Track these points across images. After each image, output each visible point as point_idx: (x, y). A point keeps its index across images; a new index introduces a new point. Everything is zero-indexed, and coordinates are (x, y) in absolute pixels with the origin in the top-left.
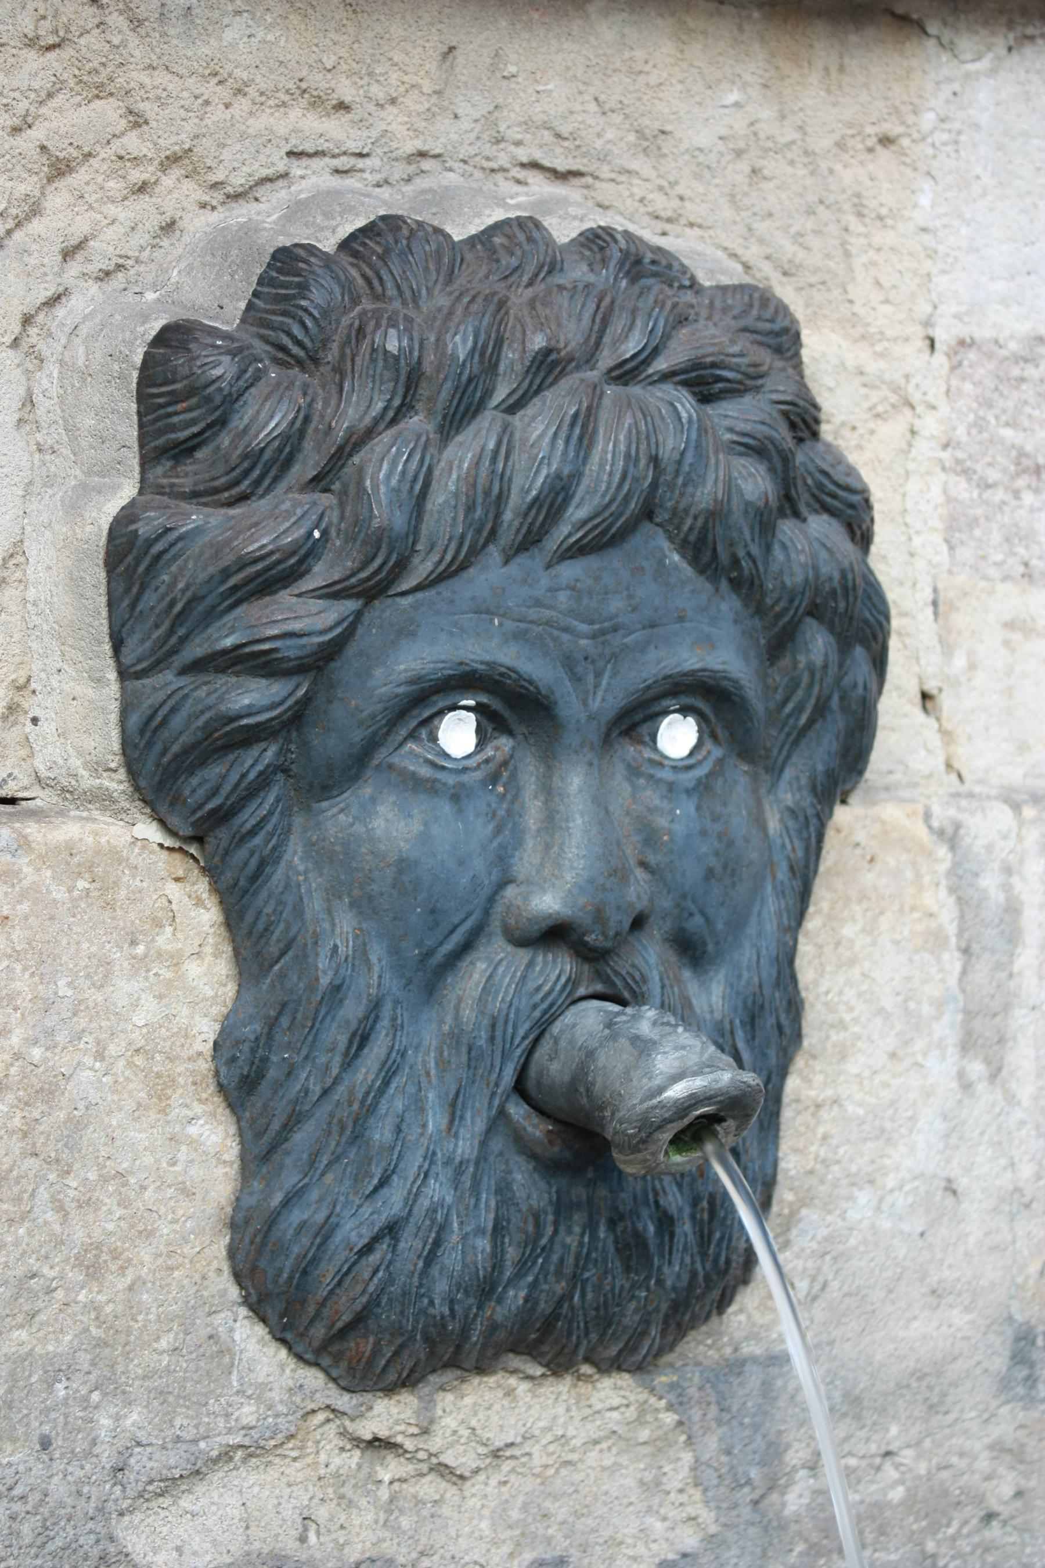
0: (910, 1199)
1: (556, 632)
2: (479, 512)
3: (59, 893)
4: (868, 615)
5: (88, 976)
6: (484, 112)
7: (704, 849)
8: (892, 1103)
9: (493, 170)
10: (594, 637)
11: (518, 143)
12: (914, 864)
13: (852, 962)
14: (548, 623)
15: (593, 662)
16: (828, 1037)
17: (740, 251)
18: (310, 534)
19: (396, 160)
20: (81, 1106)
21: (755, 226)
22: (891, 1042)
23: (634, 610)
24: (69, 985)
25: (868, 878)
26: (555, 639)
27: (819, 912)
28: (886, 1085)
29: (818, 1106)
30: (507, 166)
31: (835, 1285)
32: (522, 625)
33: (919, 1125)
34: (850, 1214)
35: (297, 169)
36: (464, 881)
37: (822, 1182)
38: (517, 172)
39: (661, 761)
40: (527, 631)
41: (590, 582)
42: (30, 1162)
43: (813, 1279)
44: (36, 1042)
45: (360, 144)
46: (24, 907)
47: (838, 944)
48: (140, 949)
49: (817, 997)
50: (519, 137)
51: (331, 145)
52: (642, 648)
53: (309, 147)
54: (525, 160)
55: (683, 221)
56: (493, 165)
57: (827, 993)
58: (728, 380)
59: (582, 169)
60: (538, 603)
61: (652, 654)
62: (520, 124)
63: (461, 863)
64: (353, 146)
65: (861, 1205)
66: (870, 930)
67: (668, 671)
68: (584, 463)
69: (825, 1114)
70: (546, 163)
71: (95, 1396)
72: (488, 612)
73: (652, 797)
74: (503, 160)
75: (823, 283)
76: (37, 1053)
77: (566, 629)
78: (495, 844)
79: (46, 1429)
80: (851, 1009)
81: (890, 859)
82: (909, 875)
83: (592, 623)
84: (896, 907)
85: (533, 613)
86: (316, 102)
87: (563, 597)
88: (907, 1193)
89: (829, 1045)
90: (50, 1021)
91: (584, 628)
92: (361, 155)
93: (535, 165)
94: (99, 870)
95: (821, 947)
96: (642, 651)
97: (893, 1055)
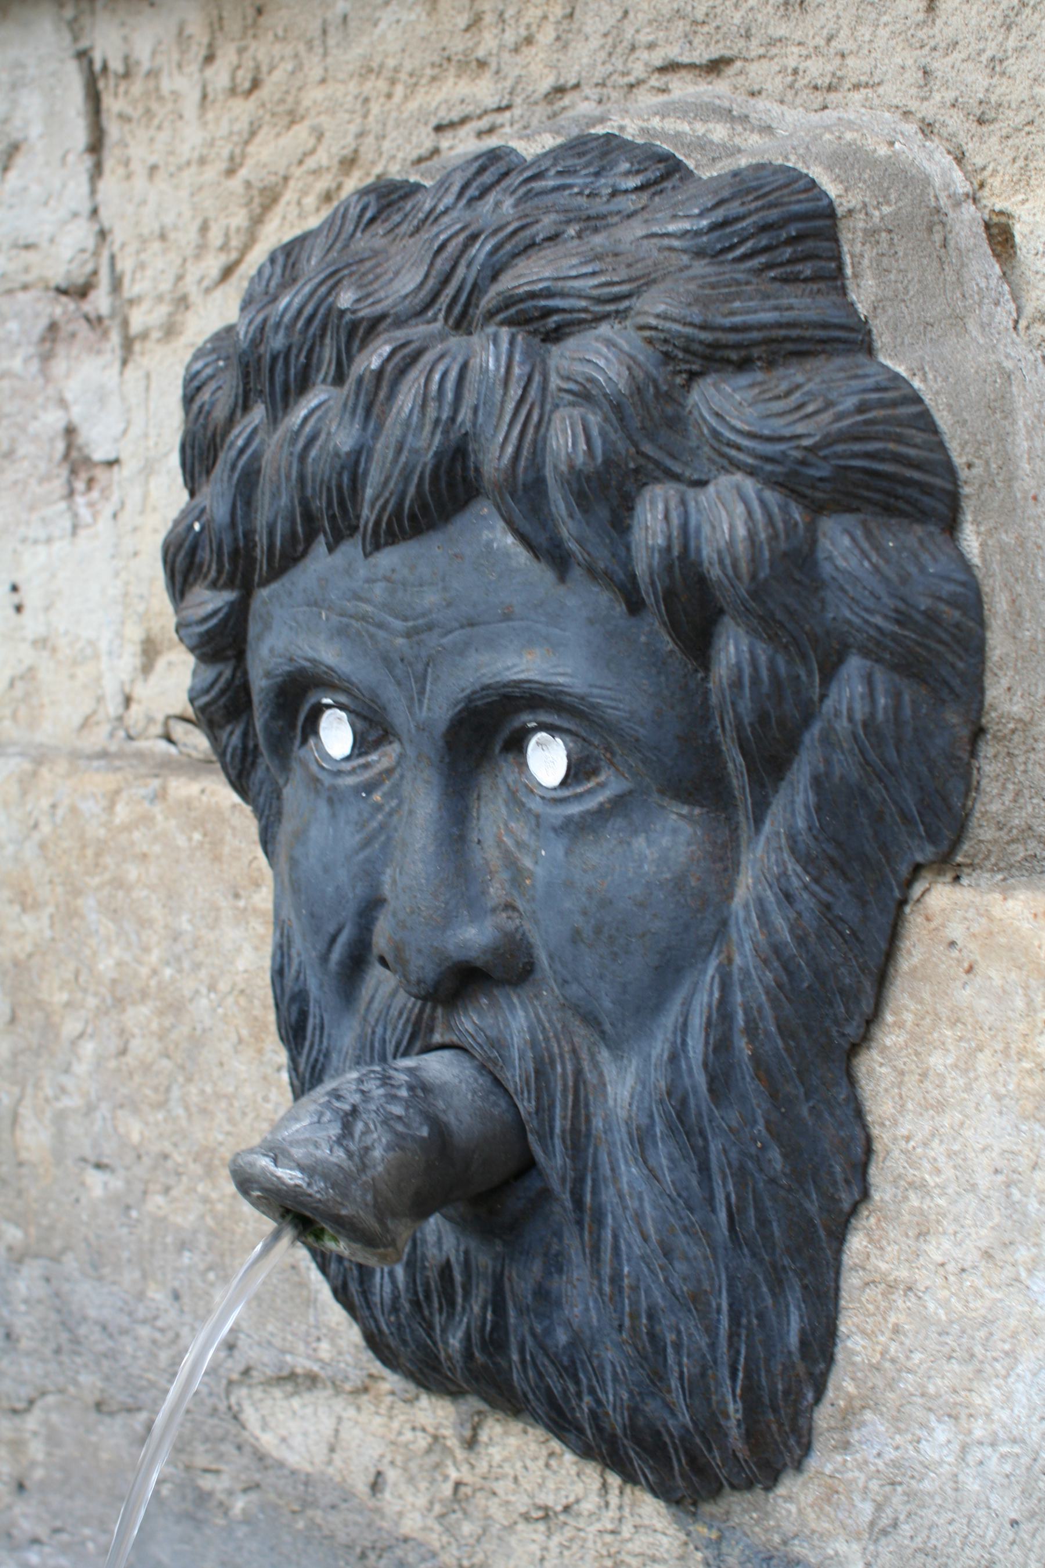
0: (1008, 1468)
1: (373, 629)
2: (284, 500)
3: (181, 841)
4: (848, 614)
5: (203, 917)
6: (612, 21)
7: (567, 905)
8: (986, 1322)
9: (631, 86)
10: (408, 634)
11: (651, 46)
12: (1026, 987)
13: (940, 1107)
14: (364, 618)
15: (411, 664)
16: (906, 1198)
17: (913, 105)
18: (191, 527)
19: (536, 103)
20: (199, 1027)
21: (935, 65)
22: (984, 1236)
23: (449, 605)
24: (190, 921)
25: (964, 995)
26: (372, 636)
27: (900, 1025)
28: (978, 1294)
29: (891, 1287)
30: (643, 76)
31: (906, 1529)
32: (345, 620)
33: (1020, 1370)
34: (924, 1445)
35: (445, 142)
36: (330, 889)
37: (891, 1386)
38: (655, 81)
39: (532, 787)
40: (348, 626)
41: (406, 572)
42: (165, 1063)
43: (879, 1507)
44: (168, 963)
45: (497, 99)
46: (157, 849)
47: (924, 1075)
48: (241, 903)
49: (895, 1139)
50: (651, 38)
51: (471, 108)
52: (462, 649)
53: (455, 116)
54: (659, 63)
55: (847, 85)
56: (631, 79)
57: (908, 1139)
58: (564, 311)
59: (728, 53)
60: (357, 597)
61: (474, 658)
62: (650, 22)
63: (326, 870)
64: (491, 102)
65: (939, 1441)
66: (965, 1066)
67: (487, 681)
68: (375, 437)
69: (898, 1297)
70: (685, 59)
71: (211, 1276)
72: (316, 604)
73: (521, 830)
74: (638, 70)
75: (1031, 123)
76: (168, 972)
77: (381, 626)
78: (361, 856)
79: (176, 1284)
80: (938, 1171)
81: (994, 974)
82: (1020, 1003)
83: (406, 619)
84: (999, 1047)
85: (350, 606)
86: (463, 66)
87: (379, 590)
88: (1003, 1457)
89: (905, 1208)
90: (178, 948)
91: (398, 624)
92: (499, 109)
93: (671, 67)
94: (209, 826)
95: (902, 1073)
96: (462, 654)
97: (987, 1255)
